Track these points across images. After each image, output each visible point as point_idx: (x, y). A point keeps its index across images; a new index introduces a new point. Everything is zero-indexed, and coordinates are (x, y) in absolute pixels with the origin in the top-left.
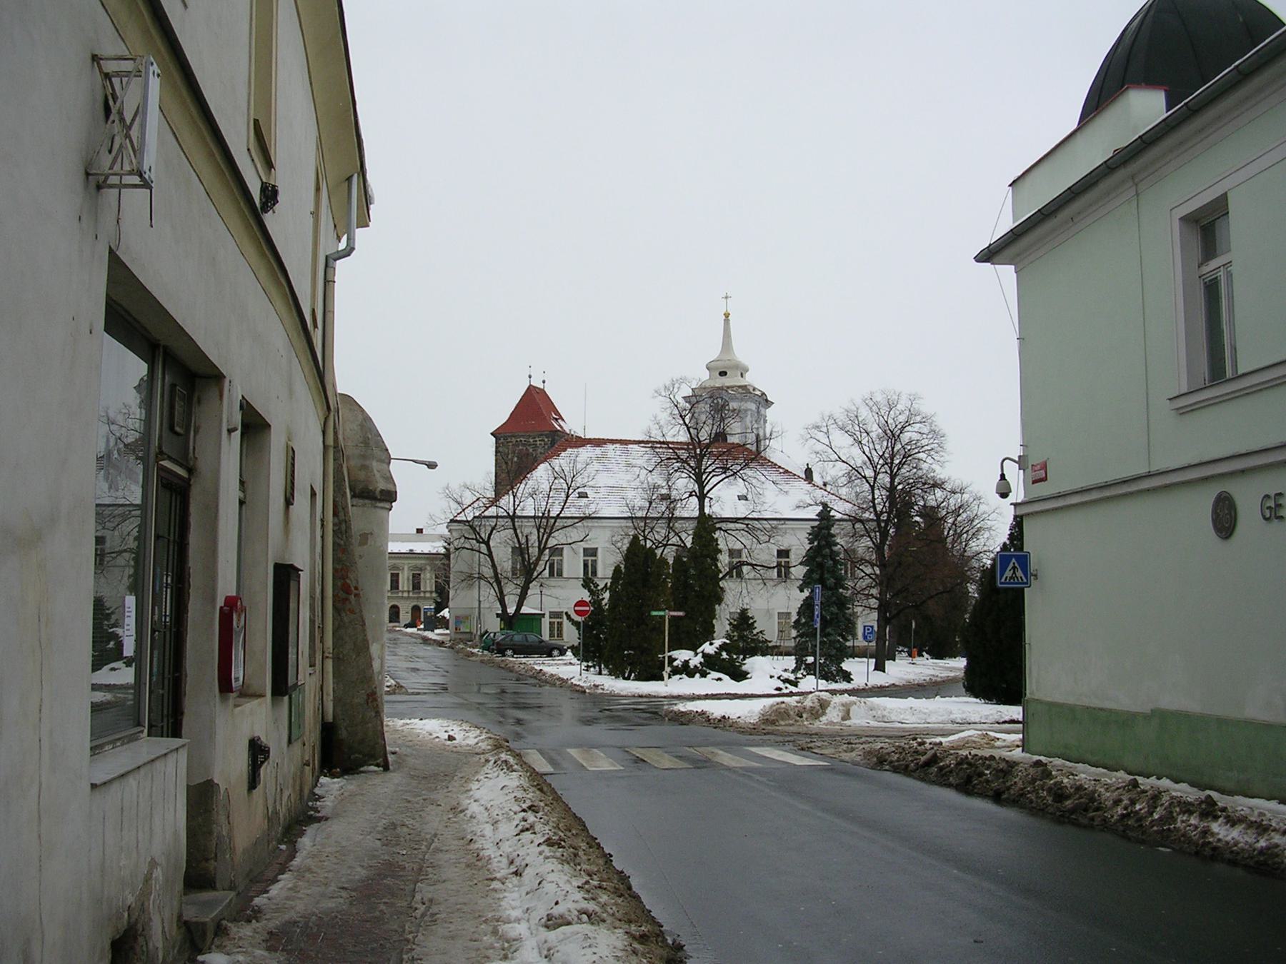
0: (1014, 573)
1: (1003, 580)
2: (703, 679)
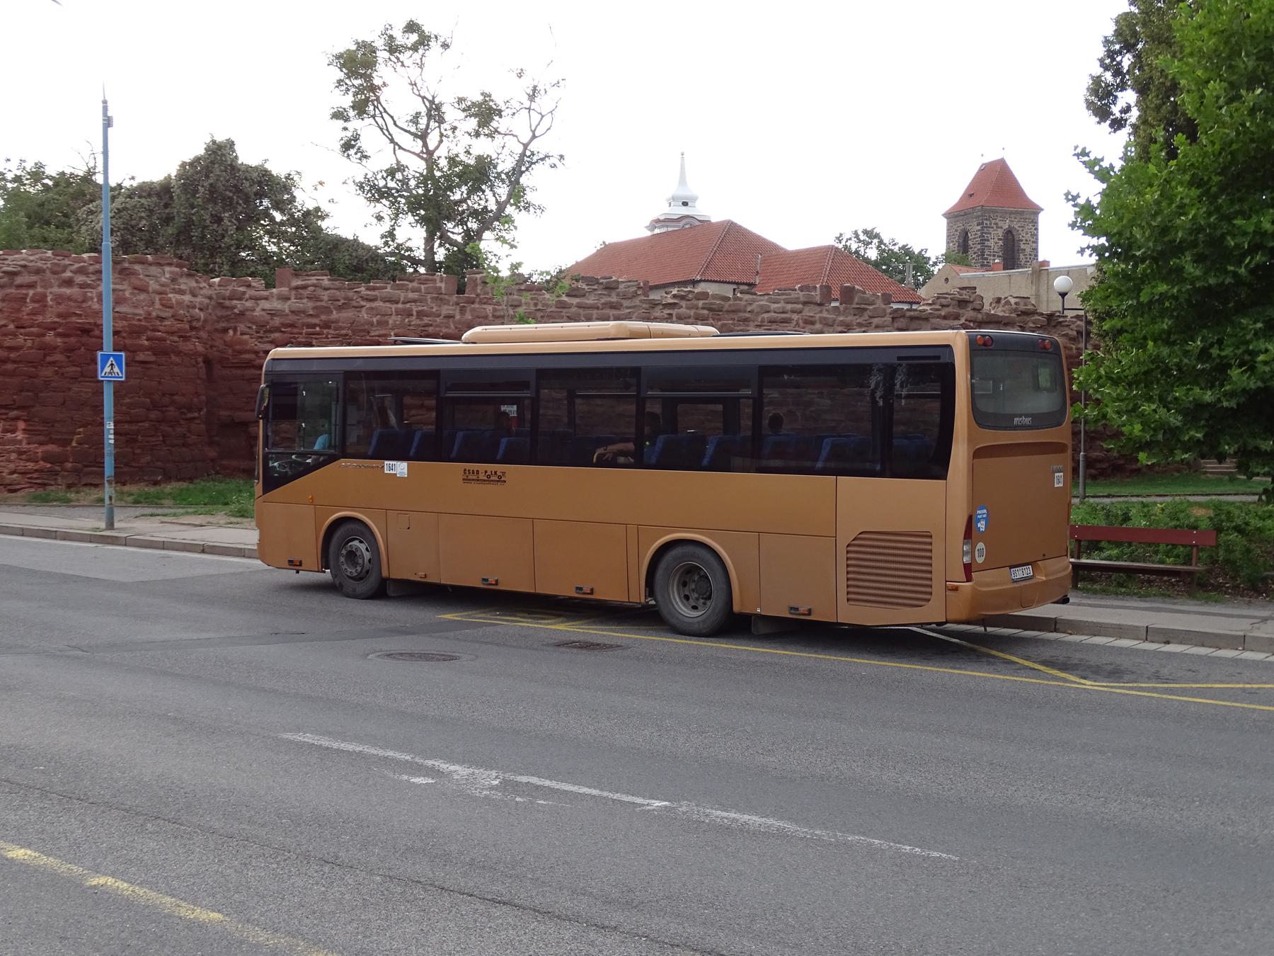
0: (112, 369)
1: (103, 375)
2: (220, 138)
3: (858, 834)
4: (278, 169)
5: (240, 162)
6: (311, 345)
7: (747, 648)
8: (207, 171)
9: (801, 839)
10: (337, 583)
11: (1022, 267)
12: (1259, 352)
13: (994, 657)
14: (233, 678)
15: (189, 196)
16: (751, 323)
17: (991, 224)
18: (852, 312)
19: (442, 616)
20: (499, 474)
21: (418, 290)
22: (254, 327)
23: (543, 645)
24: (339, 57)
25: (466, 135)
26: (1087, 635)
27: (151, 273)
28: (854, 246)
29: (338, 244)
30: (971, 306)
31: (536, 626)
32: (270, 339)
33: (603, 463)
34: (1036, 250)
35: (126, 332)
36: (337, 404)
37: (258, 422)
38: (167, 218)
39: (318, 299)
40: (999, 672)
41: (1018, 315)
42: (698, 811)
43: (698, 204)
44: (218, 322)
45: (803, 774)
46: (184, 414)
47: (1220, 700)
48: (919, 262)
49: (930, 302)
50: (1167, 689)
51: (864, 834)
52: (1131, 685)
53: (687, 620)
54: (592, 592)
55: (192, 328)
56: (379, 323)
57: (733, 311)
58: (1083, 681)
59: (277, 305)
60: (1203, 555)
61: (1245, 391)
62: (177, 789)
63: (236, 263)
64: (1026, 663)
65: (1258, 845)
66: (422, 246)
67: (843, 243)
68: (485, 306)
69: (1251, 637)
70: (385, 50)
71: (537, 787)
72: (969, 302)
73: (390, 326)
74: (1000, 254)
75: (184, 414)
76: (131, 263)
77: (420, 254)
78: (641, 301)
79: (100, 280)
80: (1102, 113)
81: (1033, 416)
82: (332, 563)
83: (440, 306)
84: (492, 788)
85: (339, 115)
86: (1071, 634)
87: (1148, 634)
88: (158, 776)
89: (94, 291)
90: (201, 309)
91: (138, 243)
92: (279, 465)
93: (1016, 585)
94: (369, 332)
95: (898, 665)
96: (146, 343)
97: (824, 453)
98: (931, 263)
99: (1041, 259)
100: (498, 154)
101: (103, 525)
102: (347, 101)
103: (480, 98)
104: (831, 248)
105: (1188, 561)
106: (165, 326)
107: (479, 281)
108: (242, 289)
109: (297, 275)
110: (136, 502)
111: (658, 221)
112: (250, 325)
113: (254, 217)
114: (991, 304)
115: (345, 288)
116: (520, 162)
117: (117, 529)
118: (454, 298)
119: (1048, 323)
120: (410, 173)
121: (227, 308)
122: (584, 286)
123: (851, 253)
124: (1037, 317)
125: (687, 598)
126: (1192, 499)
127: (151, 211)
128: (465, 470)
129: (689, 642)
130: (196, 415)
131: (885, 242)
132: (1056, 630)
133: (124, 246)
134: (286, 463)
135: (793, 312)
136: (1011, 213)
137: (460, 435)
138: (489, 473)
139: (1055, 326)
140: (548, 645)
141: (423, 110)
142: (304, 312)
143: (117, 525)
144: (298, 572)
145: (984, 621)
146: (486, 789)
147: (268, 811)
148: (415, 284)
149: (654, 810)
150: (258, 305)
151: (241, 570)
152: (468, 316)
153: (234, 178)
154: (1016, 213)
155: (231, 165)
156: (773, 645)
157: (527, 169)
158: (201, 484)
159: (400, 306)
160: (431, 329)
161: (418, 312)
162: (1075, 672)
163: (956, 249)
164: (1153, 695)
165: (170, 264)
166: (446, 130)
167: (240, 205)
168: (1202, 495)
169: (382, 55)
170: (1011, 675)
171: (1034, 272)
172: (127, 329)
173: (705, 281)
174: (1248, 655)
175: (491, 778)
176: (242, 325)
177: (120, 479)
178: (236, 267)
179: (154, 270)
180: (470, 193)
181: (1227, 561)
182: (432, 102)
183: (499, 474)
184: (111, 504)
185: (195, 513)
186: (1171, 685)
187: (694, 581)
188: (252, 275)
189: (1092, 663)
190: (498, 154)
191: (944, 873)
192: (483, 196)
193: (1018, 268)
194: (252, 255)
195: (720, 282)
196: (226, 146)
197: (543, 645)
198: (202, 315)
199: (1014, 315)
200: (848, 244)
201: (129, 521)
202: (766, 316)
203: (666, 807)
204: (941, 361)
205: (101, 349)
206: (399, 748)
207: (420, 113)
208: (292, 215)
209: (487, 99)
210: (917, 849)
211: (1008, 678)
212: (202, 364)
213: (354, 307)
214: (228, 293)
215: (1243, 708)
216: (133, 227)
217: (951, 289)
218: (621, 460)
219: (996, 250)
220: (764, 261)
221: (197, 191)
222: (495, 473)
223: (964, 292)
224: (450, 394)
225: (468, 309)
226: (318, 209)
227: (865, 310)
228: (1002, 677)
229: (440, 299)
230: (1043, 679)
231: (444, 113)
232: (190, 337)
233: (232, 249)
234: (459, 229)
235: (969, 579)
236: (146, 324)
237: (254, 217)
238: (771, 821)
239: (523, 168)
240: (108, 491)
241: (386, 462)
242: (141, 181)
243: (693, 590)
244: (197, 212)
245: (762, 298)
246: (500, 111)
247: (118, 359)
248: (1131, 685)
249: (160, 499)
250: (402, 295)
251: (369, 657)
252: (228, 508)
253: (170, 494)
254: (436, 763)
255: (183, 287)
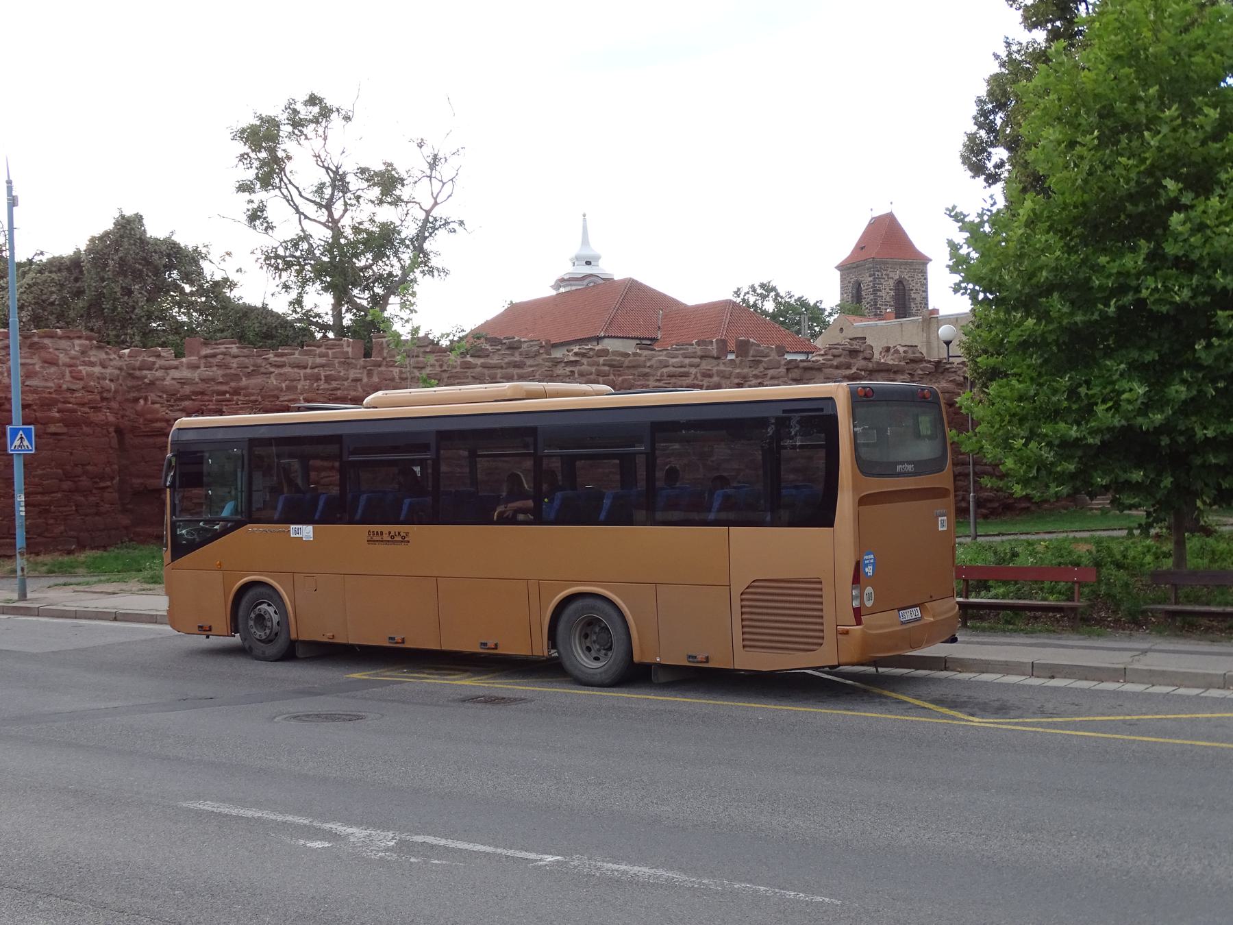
0: (21, 442)
1: (13, 448)
2: (128, 213)
3: (744, 882)
4: (186, 240)
5: (148, 236)
6: (221, 413)
7: (647, 697)
8: (117, 244)
9: (689, 889)
10: (247, 646)
11: (914, 316)
12: (1124, 392)
13: (886, 697)
14: (138, 747)
15: (99, 270)
16: (651, 378)
17: (882, 275)
18: (748, 364)
19: (351, 676)
20: (402, 534)
21: (326, 355)
22: (165, 396)
23: (448, 701)
24: (243, 131)
25: (370, 203)
26: (975, 672)
27: (61, 347)
28: (752, 299)
29: (247, 312)
30: (861, 356)
31: (442, 682)
32: (181, 407)
33: (505, 520)
34: (926, 298)
35: (36, 405)
36: (242, 471)
37: (165, 490)
38: (77, 292)
39: (227, 367)
40: (890, 712)
41: (907, 363)
42: (590, 865)
43: (601, 263)
44: (129, 392)
45: (695, 823)
46: (97, 483)
47: (1102, 733)
48: (815, 313)
49: (822, 352)
50: (1039, 723)
51: (750, 881)
52: (1017, 720)
53: (589, 671)
54: (496, 647)
55: (103, 399)
56: (288, 388)
57: (634, 367)
58: (971, 718)
59: (186, 374)
60: (1086, 590)
61: (1110, 429)
62: (72, 864)
63: (147, 334)
64: (917, 702)
65: (1131, 877)
66: (330, 312)
67: (742, 296)
68: (391, 369)
69: (1131, 669)
70: (288, 124)
71: (433, 847)
72: (860, 351)
73: (299, 391)
74: (892, 303)
75: (97, 483)
76: (40, 337)
77: (329, 320)
78: (543, 359)
79: (9, 354)
80: (977, 169)
81: (916, 463)
82: (241, 627)
83: (347, 370)
84: (387, 849)
85: (244, 188)
86: (960, 672)
87: (1034, 669)
88: (54, 851)
89: (4, 366)
90: (111, 380)
91: (50, 317)
92: (188, 532)
93: (904, 627)
94: (278, 398)
95: (794, 708)
96: (57, 415)
97: (716, 505)
98: (826, 313)
99: (930, 307)
100: (402, 221)
101: (15, 596)
102: (251, 174)
103: (383, 168)
104: (729, 302)
105: (1071, 599)
106: (76, 398)
107: (385, 345)
108: (151, 359)
109: (205, 344)
110: (50, 572)
111: (562, 280)
112: (160, 394)
113: (163, 288)
114: (881, 353)
115: (254, 356)
116: (423, 227)
117: (30, 600)
118: (362, 361)
119: (936, 371)
120: (316, 242)
121: (138, 378)
122: (488, 347)
123: (749, 307)
124: (925, 364)
125: (589, 649)
126: (1078, 535)
127: (62, 286)
128: (369, 531)
129: (592, 693)
130: (109, 483)
131: (781, 294)
132: (946, 669)
133: (37, 320)
134: (194, 530)
135: (691, 365)
136: (901, 264)
137: (363, 498)
138: (393, 534)
139: (942, 373)
140: (454, 701)
141: (327, 180)
142: (213, 380)
143: (29, 596)
144: (208, 637)
145: (876, 663)
146: (381, 851)
147: (162, 883)
148: (323, 350)
149: (546, 865)
150: (168, 374)
151: (152, 637)
152: (376, 379)
153: (143, 251)
154: (906, 264)
155: (140, 239)
156: (673, 693)
157: (430, 234)
158: (113, 552)
159: (308, 371)
160: (339, 393)
161: (326, 377)
162: (963, 710)
163: (850, 300)
164: (1038, 730)
165: (79, 337)
166: (350, 199)
167: (150, 277)
168: (1088, 531)
169: (286, 129)
170: (902, 715)
171: (924, 320)
172: (38, 402)
173: (608, 337)
174: (1129, 687)
175: (387, 839)
176: (152, 395)
177: (33, 548)
178: (148, 338)
179: (64, 344)
180: (375, 260)
181: (1108, 595)
182: (336, 173)
183: (402, 534)
184: (23, 575)
185: (108, 581)
186: (1055, 720)
187: (595, 633)
188: (163, 345)
189: (980, 700)
190: (402, 221)
191: (826, 918)
192: (388, 262)
193: (910, 316)
194: (163, 325)
195: (623, 338)
196: (135, 221)
197: (448, 701)
198: (113, 386)
199: (903, 363)
200: (746, 298)
201: (42, 592)
202: (665, 370)
203: (558, 861)
204: (825, 413)
205: (10, 423)
206: (298, 812)
207: (325, 184)
208: (201, 286)
209: (390, 168)
210: (801, 895)
211: (899, 717)
212: (113, 434)
213: (262, 373)
214: (138, 364)
215: (1123, 740)
216: (43, 301)
217: (842, 339)
218: (521, 517)
219: (888, 299)
220: (665, 316)
221: (107, 265)
222: (399, 533)
223: (855, 342)
224: (353, 458)
225: (375, 372)
226: (226, 280)
227: (761, 362)
228: (893, 717)
229: (347, 364)
230: (933, 718)
231: (348, 183)
232: (101, 407)
233: (143, 320)
234: (367, 294)
235: (859, 623)
236: (57, 396)
237: (163, 288)
238: (660, 872)
239: (427, 234)
240: (20, 562)
241: (292, 526)
242: (51, 256)
243: (594, 642)
244: (108, 285)
245: (661, 353)
246: (402, 180)
247: (25, 431)
248: (1017, 720)
249: (74, 568)
250: (310, 361)
251: (276, 720)
252: (141, 575)
253: (83, 563)
254: (334, 826)
255: (92, 359)
